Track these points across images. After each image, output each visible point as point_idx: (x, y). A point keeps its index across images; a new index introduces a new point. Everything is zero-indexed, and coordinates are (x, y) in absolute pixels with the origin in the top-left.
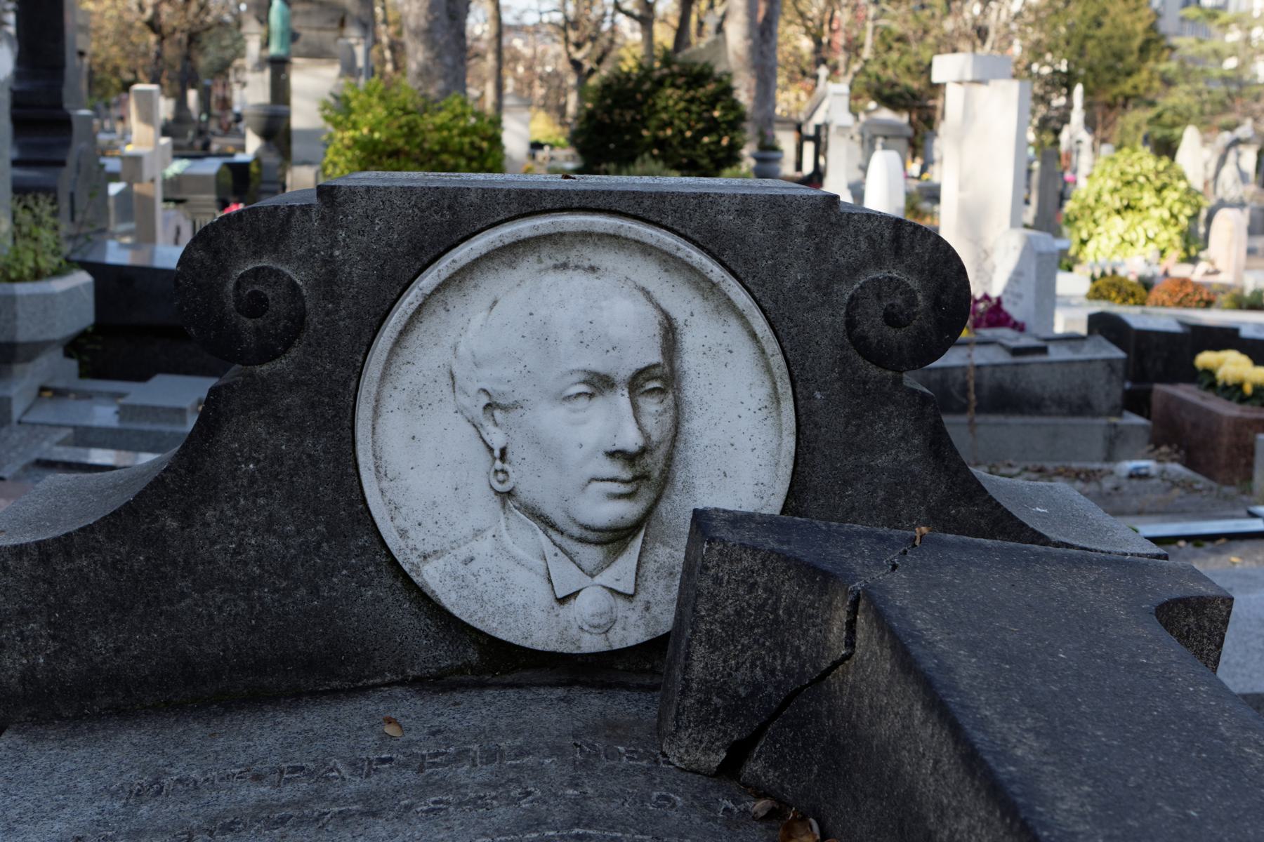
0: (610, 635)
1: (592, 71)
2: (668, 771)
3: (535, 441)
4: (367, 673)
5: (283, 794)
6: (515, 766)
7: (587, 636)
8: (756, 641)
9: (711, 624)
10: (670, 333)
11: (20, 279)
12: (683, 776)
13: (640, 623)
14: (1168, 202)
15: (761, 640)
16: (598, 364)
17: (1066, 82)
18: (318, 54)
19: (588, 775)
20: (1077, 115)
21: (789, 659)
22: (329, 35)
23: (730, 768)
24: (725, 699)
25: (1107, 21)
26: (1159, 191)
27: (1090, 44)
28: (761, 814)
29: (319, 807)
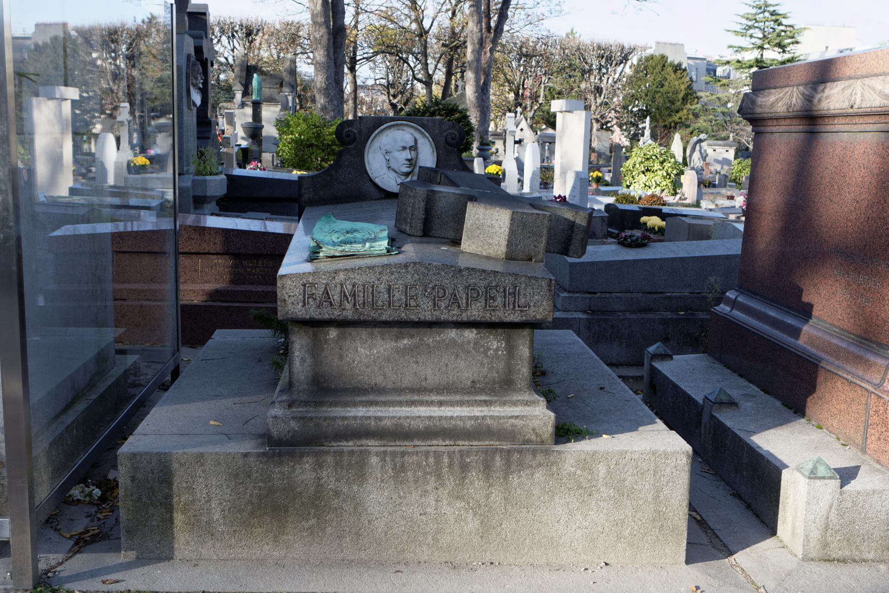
1: (402, 109)
3: (394, 158)
10: (416, 141)
11: (206, 175)
14: (666, 168)
16: (404, 145)
17: (642, 115)
18: (271, 100)
20: (647, 132)
22: (275, 91)
25: (666, 84)
26: (662, 163)
27: (657, 96)
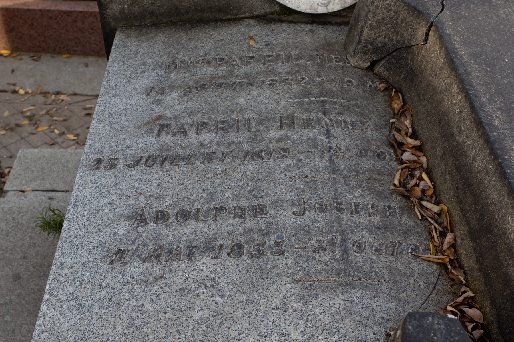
0: (328, 7)
2: (349, 67)
4: (240, 13)
5: (219, 72)
6: (297, 64)
7: (320, 8)
8: (388, 29)
9: (372, 21)
12: (355, 70)
13: (339, 3)
15: (390, 29)
19: (323, 70)
21: (399, 37)
23: (371, 68)
24: (373, 46)
28: (382, 89)
29: (232, 79)
